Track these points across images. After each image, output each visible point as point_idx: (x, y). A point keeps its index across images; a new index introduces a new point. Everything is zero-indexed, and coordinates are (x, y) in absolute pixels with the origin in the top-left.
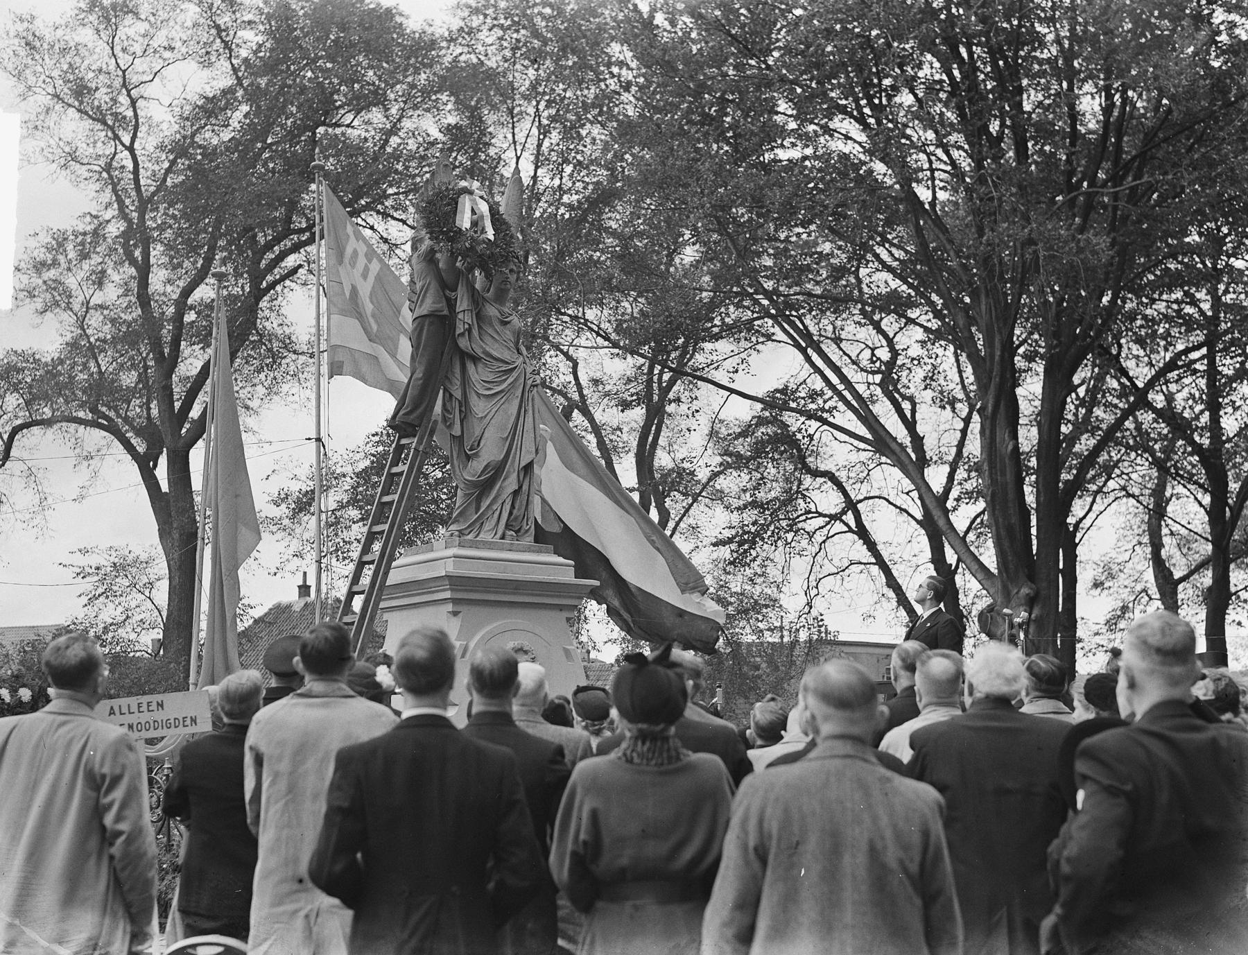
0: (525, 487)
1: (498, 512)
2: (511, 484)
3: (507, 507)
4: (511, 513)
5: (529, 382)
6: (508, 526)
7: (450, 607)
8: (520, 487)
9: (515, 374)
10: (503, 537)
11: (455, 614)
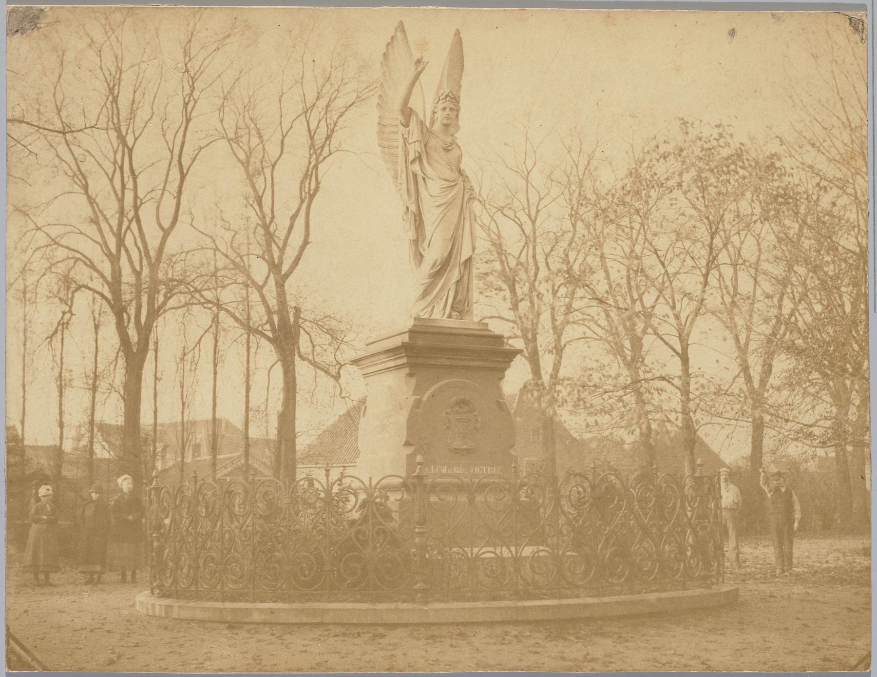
0: (466, 278)
1: (444, 298)
2: (455, 275)
3: (452, 295)
4: (455, 298)
5: (467, 197)
6: (452, 308)
7: (407, 370)
8: (462, 277)
10: (450, 316)
11: (411, 375)
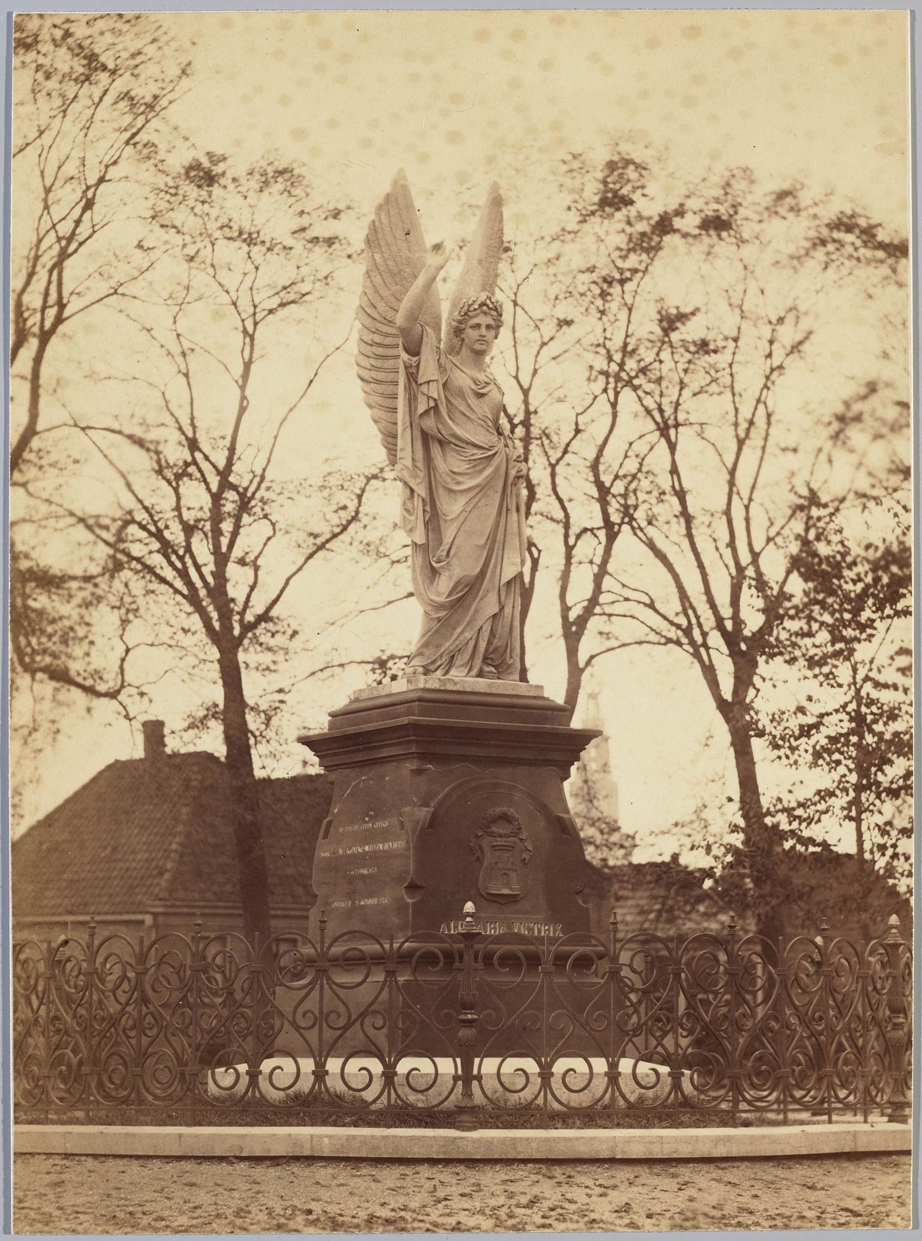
5: (513, 473)
6: (486, 659)
8: (502, 609)
9: (497, 460)
